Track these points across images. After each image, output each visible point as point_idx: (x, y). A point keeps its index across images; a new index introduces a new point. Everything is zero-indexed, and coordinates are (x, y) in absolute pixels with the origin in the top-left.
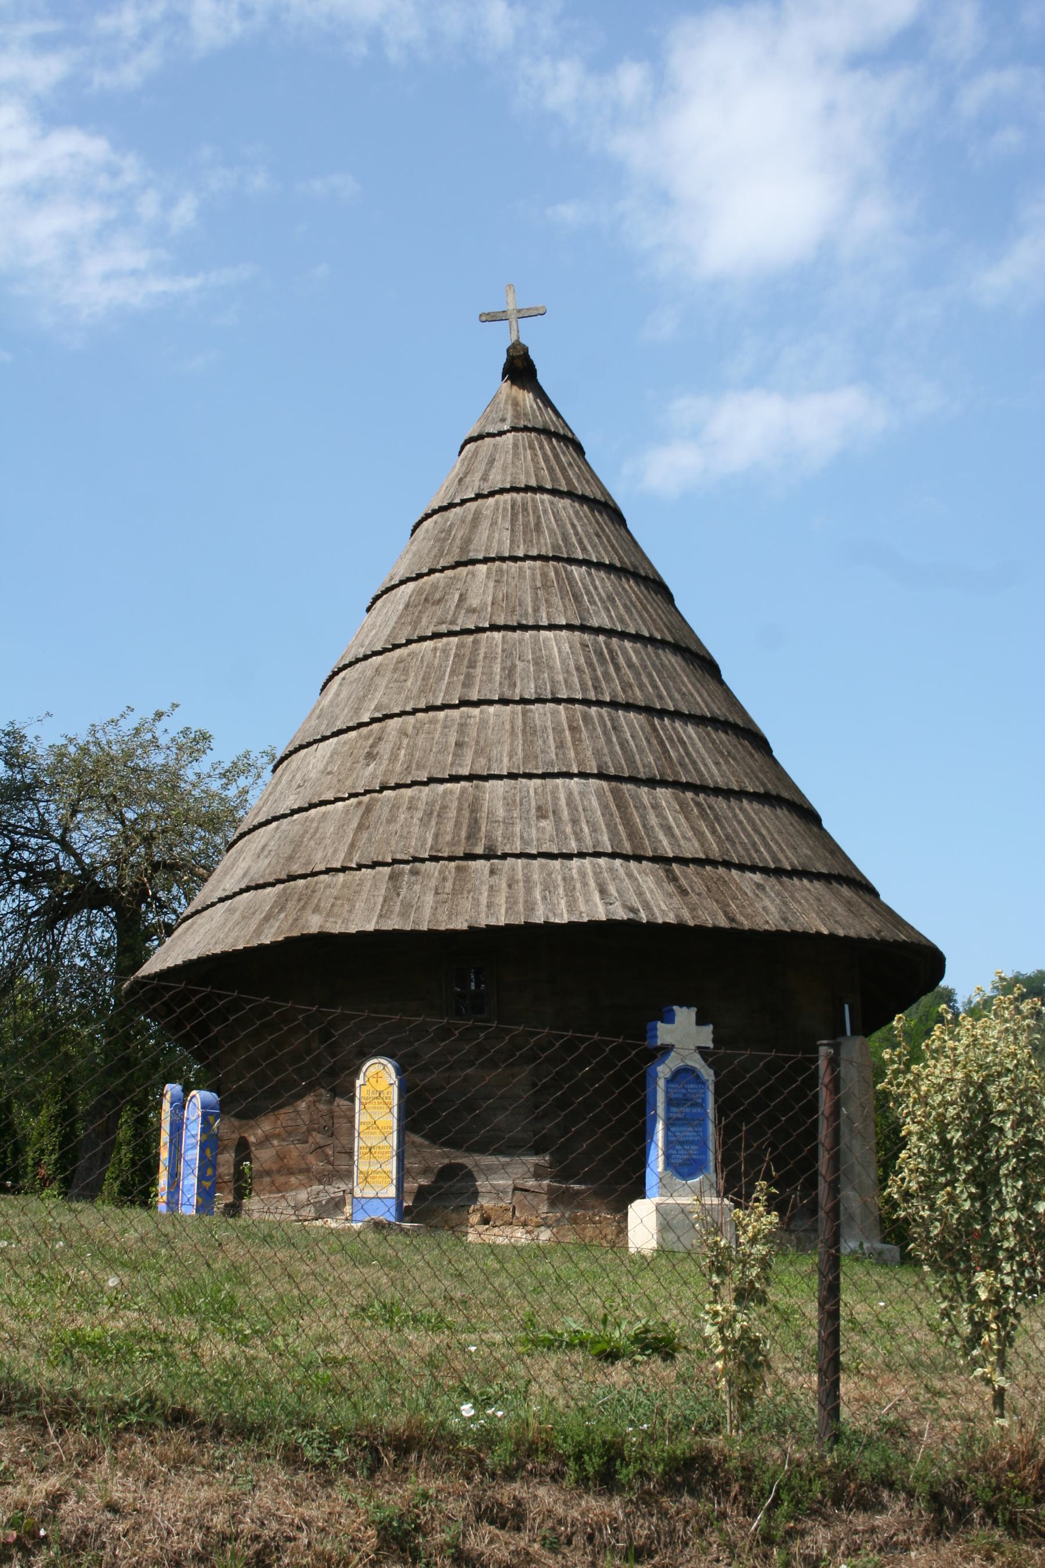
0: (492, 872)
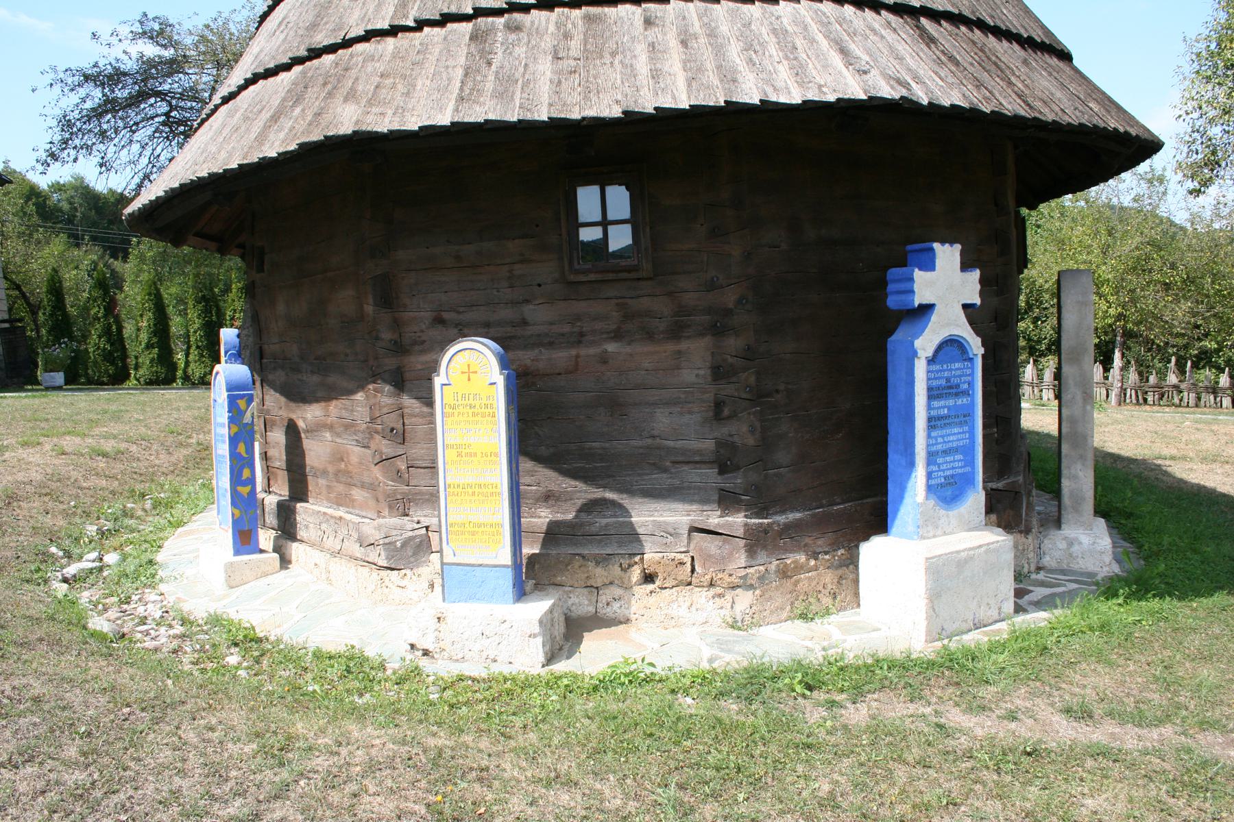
0: (648, 22)
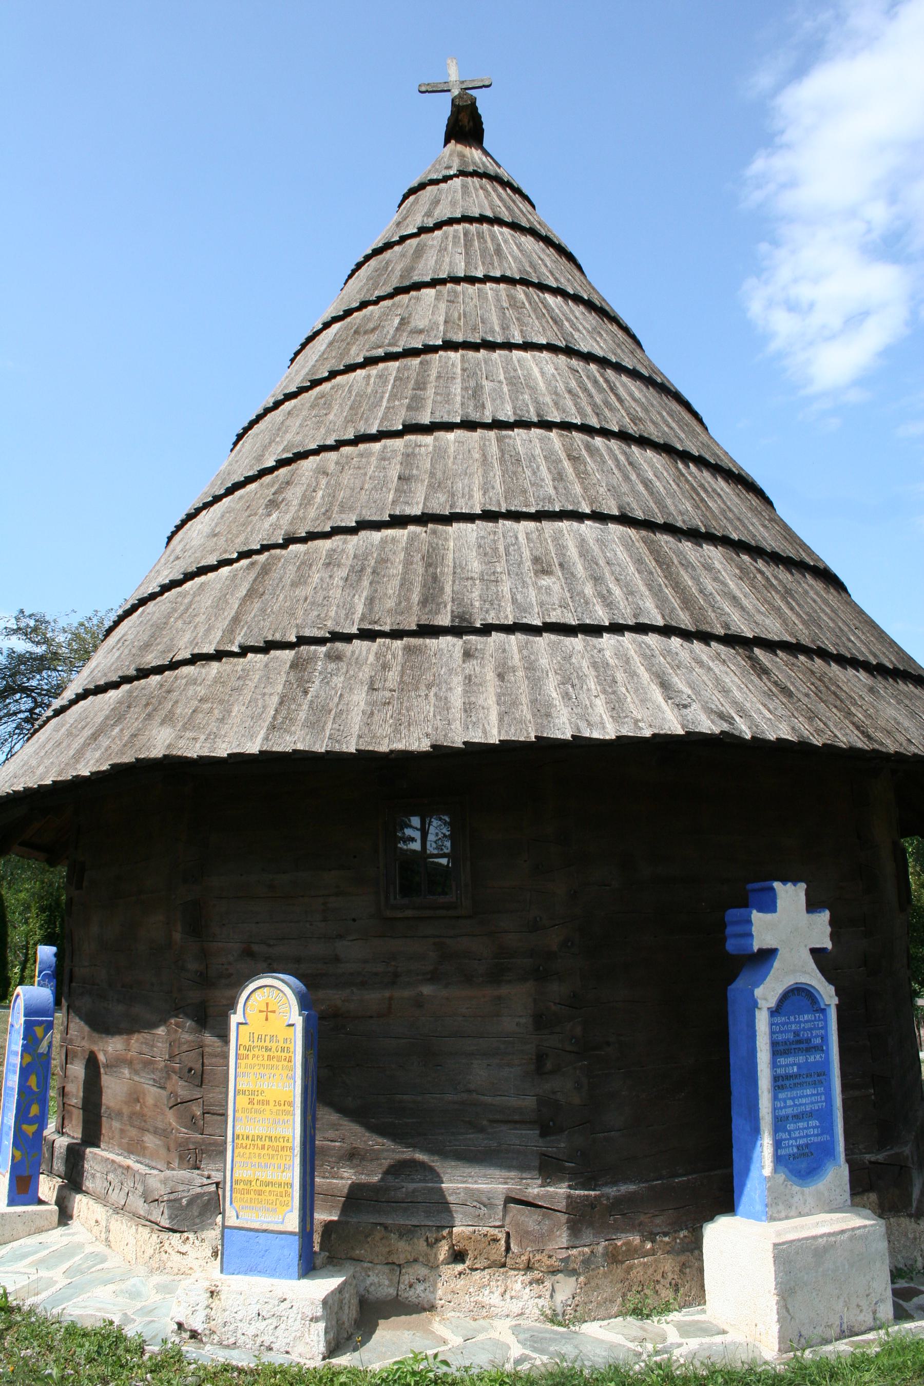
0: (468, 655)
